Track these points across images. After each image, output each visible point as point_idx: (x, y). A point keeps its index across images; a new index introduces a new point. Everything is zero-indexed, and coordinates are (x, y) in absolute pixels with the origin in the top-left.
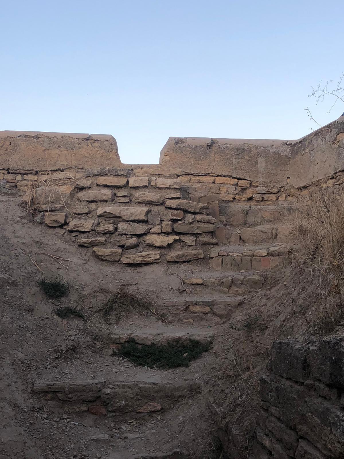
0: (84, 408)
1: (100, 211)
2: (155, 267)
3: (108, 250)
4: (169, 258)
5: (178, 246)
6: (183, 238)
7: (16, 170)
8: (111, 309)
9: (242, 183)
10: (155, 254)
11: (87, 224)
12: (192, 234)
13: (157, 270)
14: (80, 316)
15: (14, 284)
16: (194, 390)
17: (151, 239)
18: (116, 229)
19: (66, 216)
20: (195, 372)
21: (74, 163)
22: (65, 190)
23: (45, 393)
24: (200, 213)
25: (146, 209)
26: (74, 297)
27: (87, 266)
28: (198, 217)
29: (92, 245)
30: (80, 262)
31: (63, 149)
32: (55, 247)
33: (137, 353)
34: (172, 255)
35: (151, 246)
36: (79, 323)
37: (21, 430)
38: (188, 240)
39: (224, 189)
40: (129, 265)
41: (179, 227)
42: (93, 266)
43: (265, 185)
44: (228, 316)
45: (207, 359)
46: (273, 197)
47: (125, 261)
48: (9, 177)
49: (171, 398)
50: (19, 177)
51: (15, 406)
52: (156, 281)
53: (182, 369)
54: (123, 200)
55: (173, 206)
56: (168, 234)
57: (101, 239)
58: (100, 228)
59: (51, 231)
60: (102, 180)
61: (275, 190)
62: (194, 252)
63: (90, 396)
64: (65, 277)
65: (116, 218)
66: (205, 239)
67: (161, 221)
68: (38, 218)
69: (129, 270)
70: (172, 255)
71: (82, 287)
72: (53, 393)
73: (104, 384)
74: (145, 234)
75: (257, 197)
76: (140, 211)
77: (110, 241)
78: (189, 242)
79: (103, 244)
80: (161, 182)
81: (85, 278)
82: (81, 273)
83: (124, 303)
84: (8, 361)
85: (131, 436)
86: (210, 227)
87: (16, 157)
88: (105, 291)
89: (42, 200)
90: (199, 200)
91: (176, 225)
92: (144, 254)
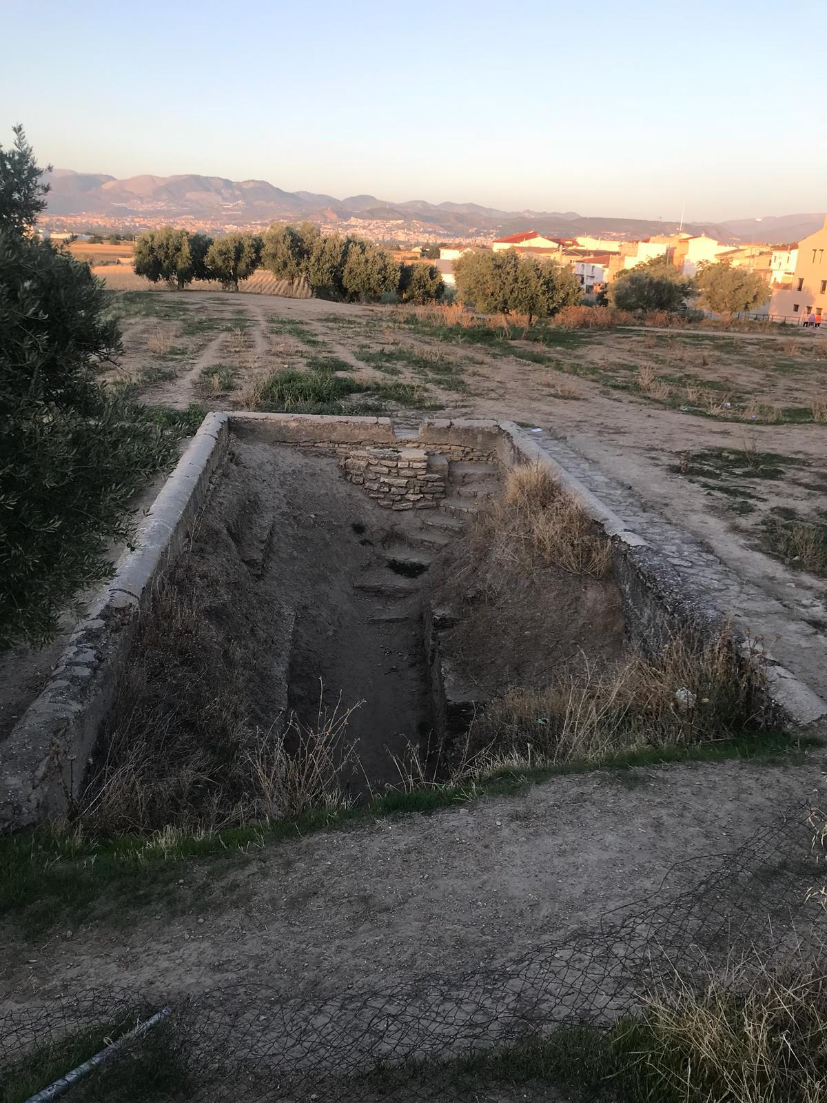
2: (410, 512)
3: (386, 503)
4: (417, 507)
7: (316, 335)
8: (386, 540)
10: (410, 505)
15: (340, 527)
16: (417, 590)
18: (390, 490)
20: (418, 582)
22: (363, 463)
25: (406, 481)
26: (368, 532)
28: (435, 484)
29: (377, 498)
34: (420, 504)
35: (409, 500)
36: (370, 547)
38: (429, 497)
42: (377, 511)
43: (481, 451)
46: (485, 459)
48: (331, 445)
49: (408, 593)
50: (336, 446)
51: (348, 594)
52: (408, 521)
53: (414, 579)
56: (417, 494)
57: (382, 496)
58: (381, 490)
59: (355, 487)
60: (383, 462)
61: (486, 455)
62: (431, 503)
64: (365, 520)
65: (390, 486)
68: (349, 478)
69: (396, 513)
70: (420, 504)
71: (372, 526)
72: (361, 588)
73: (382, 585)
75: (475, 458)
79: (383, 499)
80: (415, 465)
81: (374, 520)
82: (373, 517)
83: (393, 537)
85: (391, 608)
87: (334, 434)
88: (382, 529)
89: (351, 467)
90: (436, 472)
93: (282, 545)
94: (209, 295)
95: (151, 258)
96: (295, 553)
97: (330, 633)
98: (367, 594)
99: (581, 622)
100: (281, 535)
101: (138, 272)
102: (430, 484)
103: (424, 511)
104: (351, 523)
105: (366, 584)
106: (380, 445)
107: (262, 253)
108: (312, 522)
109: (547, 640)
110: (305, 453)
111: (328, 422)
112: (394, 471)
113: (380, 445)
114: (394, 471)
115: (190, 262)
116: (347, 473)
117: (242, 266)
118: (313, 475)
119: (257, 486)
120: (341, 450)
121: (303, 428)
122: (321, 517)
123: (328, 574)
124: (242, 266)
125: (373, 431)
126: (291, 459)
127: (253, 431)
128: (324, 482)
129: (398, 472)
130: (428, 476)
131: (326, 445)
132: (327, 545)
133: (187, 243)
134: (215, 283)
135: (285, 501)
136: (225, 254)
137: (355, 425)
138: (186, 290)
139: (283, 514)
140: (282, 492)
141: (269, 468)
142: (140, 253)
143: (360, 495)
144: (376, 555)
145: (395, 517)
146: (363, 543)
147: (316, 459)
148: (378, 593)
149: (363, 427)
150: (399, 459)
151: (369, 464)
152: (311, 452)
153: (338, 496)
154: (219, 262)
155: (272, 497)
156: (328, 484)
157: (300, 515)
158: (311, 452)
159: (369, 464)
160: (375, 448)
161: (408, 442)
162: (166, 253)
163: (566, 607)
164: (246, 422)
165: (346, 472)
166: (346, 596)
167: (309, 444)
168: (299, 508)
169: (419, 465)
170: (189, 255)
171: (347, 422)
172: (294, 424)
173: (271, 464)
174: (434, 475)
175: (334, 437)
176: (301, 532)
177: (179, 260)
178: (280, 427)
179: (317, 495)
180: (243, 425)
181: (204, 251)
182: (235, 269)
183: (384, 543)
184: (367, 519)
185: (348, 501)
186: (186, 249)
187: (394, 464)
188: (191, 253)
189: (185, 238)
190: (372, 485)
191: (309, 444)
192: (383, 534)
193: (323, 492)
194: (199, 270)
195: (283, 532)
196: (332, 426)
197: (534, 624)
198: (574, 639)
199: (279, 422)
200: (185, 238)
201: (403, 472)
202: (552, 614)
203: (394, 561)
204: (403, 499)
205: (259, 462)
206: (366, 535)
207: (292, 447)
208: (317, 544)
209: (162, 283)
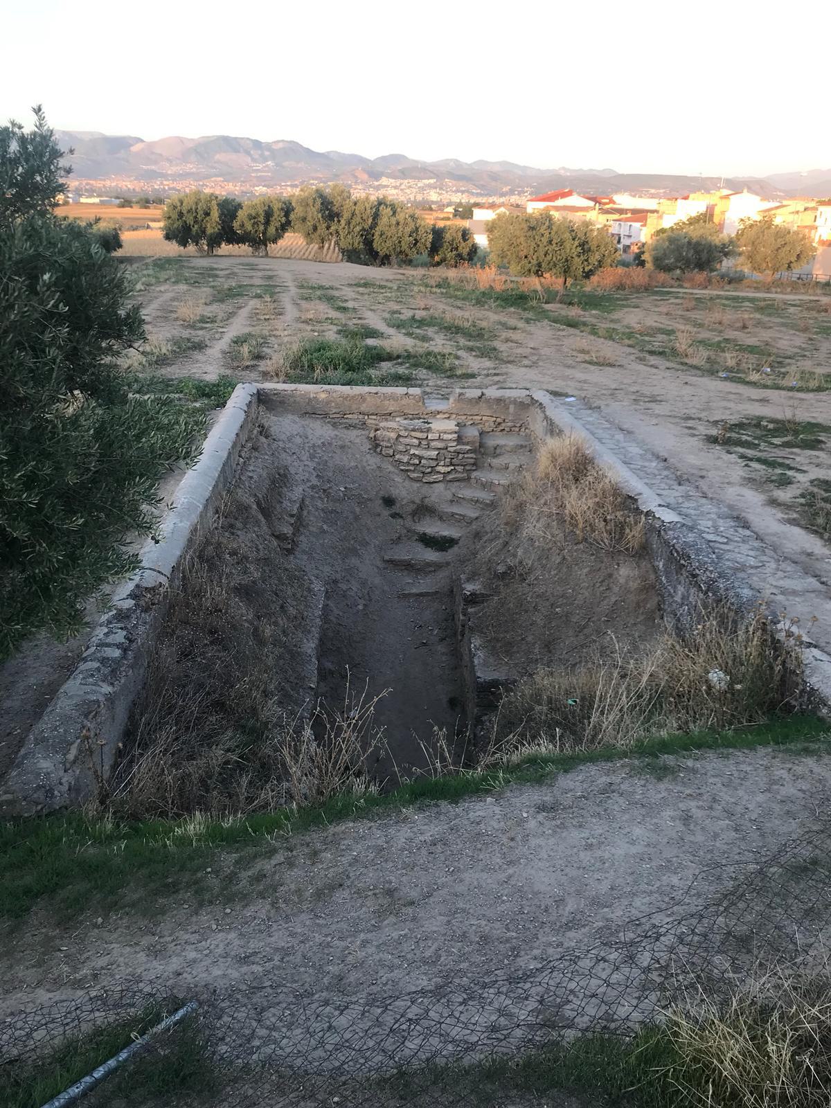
1: (412, 452)
2: (440, 484)
3: (416, 475)
7: (346, 301)
9: (499, 420)
10: (440, 477)
14: (401, 517)
15: (370, 500)
16: (448, 564)
17: (439, 469)
22: (393, 435)
26: (398, 505)
29: (407, 471)
33: (428, 541)
34: (450, 477)
35: (439, 472)
38: (460, 468)
39: (487, 424)
42: (407, 483)
44: (470, 523)
45: (455, 549)
48: (361, 417)
49: (438, 566)
52: (438, 494)
57: (412, 468)
60: (413, 434)
65: (420, 458)
66: (468, 468)
68: (378, 450)
69: (426, 485)
70: (450, 477)
72: (391, 561)
77: (419, 471)
80: (446, 437)
81: (404, 493)
82: (403, 490)
83: (424, 510)
86: (472, 461)
88: (413, 502)
90: (468, 444)
95: (180, 223)
99: (613, 599)
107: (292, 217)
110: (334, 425)
112: (424, 442)
114: (424, 442)
116: (377, 445)
117: (272, 230)
118: (342, 447)
119: (286, 459)
120: (371, 421)
124: (272, 230)
125: (403, 402)
126: (320, 431)
127: (282, 402)
129: (428, 444)
132: (357, 518)
133: (216, 207)
134: (245, 248)
135: (315, 474)
140: (312, 465)
141: (298, 440)
142: (169, 218)
143: (391, 468)
145: (425, 490)
147: (346, 431)
150: (429, 430)
151: (399, 436)
152: (341, 424)
153: (368, 468)
158: (341, 424)
159: (399, 436)
161: (439, 413)
162: (196, 217)
165: (375, 444)
168: (329, 481)
169: (450, 437)
172: (323, 396)
175: (364, 408)
176: (330, 506)
177: (208, 226)
178: (310, 399)
181: (233, 216)
186: (215, 214)
187: (425, 435)
193: (353, 464)
194: (228, 234)
200: (214, 202)
204: (433, 471)
206: (396, 509)
208: (347, 518)
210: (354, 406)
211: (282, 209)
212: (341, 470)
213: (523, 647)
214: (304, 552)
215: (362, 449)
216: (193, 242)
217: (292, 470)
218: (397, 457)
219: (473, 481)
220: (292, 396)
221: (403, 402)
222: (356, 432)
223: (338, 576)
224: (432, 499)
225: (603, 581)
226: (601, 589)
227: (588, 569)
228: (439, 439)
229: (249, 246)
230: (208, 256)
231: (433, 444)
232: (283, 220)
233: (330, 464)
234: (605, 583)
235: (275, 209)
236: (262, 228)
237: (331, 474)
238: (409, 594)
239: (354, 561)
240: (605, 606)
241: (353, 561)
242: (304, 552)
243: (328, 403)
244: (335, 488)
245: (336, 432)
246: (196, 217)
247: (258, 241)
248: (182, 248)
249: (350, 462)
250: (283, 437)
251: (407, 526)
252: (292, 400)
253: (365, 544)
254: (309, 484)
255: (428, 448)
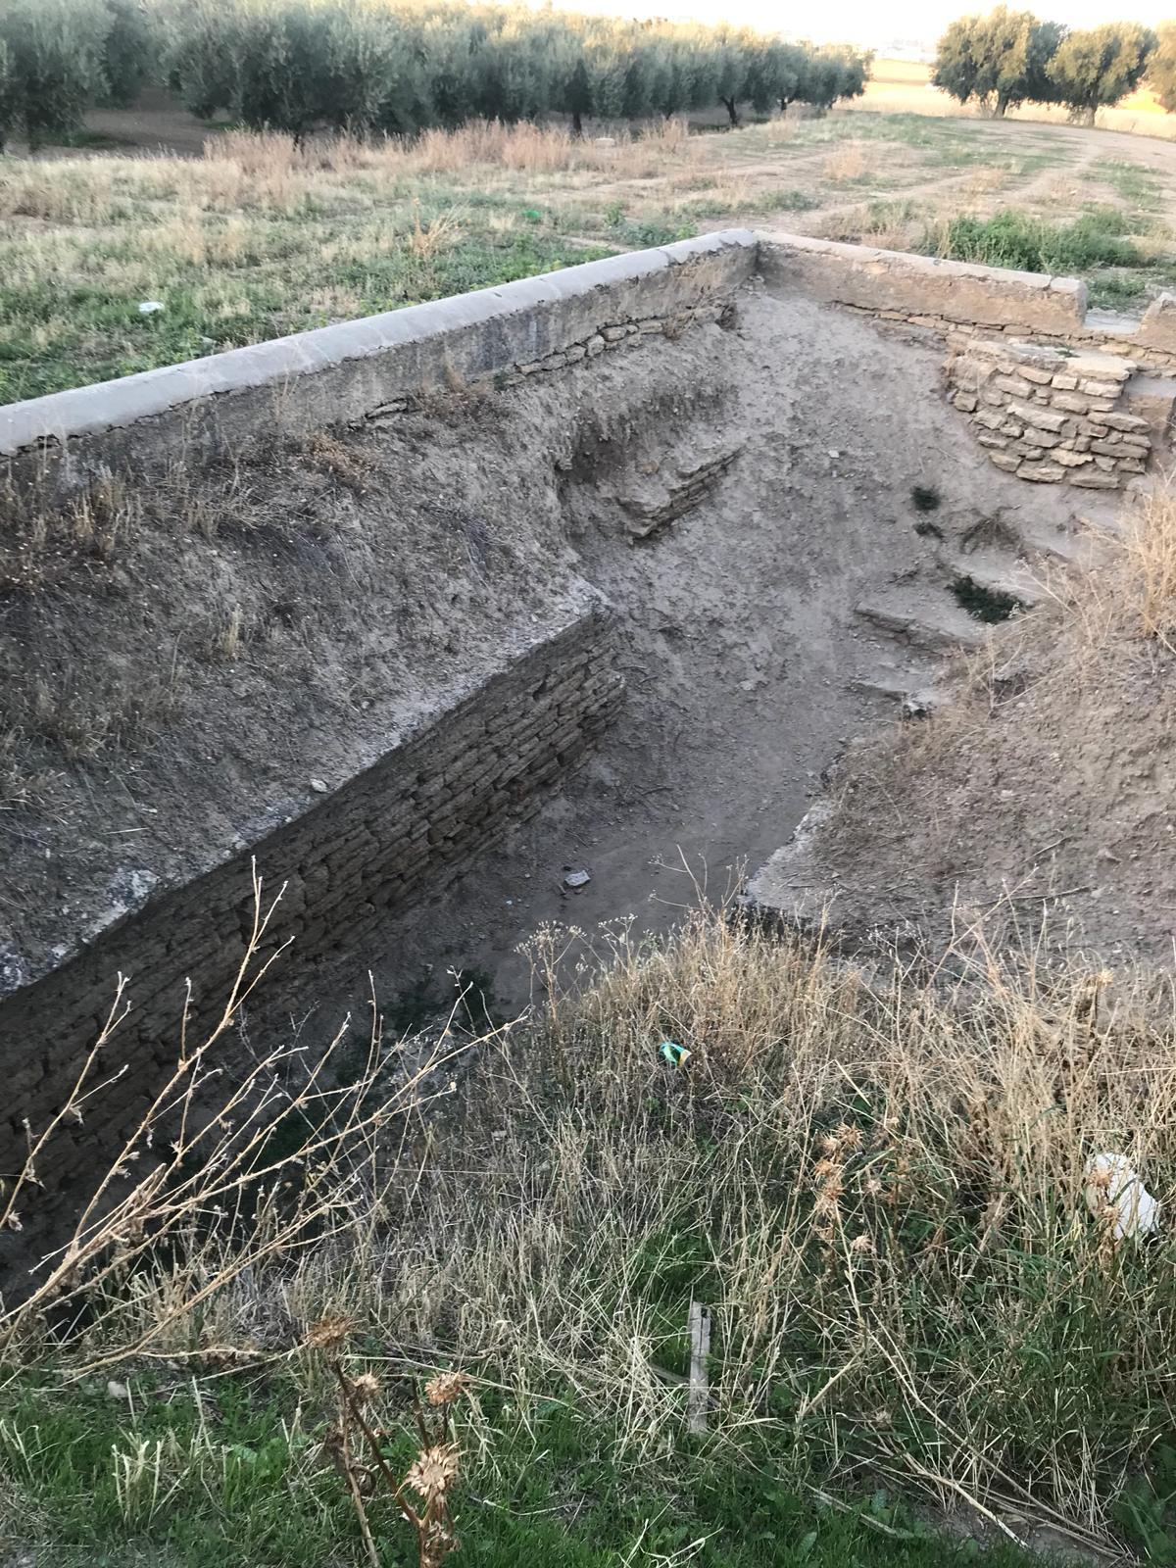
0: (891, 635)
1: (1010, 410)
5: (1089, 468)
6: (1099, 460)
10: (1057, 473)
11: (994, 420)
12: (1113, 457)
13: (1051, 493)
15: (888, 488)
18: (1022, 434)
19: (977, 403)
21: (1020, 318)
22: (985, 369)
23: (864, 614)
24: (1132, 432)
25: (1062, 418)
26: (942, 511)
27: (976, 473)
28: (1127, 437)
29: (992, 446)
30: (972, 465)
31: (1011, 298)
32: (953, 440)
34: (1079, 477)
37: (831, 642)
38: (1105, 463)
40: (1024, 479)
41: (1098, 445)
42: (982, 475)
47: (1021, 474)
48: (941, 325)
50: (952, 327)
51: (836, 621)
54: (1040, 401)
55: (1096, 421)
56: (1081, 452)
57: (1002, 443)
58: (1004, 430)
59: (959, 415)
60: (1024, 370)
62: (1107, 479)
63: (899, 628)
64: (946, 485)
66: (1124, 465)
67: (1078, 434)
69: (1023, 485)
70: (1079, 477)
72: (869, 616)
73: (913, 622)
74: (1053, 448)
76: (1054, 419)
78: (1104, 467)
79: (1005, 449)
80: (1092, 387)
81: (966, 490)
82: (968, 485)
84: (847, 577)
86: (1139, 452)
87: (953, 301)
88: (976, 512)
89: (960, 372)
90: (1141, 413)
91: (1095, 443)
92: (1044, 470)
93: (737, 494)
94: (1035, 128)
95: (962, 59)
96: (757, 517)
97: (748, 685)
98: (878, 632)
99: (1147, 808)
100: (746, 475)
101: (937, 82)
102: (1115, 436)
103: (1087, 492)
104: (914, 484)
105: (883, 611)
106: (1043, 339)
107: (1150, 58)
108: (827, 463)
109: (1044, 827)
110: (884, 334)
111: (946, 273)
112: (1041, 392)
113: (1043, 339)
114: (1041, 392)
115: (1024, 70)
116: (951, 386)
117: (1110, 78)
118: (877, 377)
119: (742, 374)
120: (956, 337)
121: (892, 279)
122: (854, 459)
123: (813, 573)
124: (1110, 78)
125: (1034, 306)
126: (849, 337)
127: (797, 274)
128: (894, 395)
129: (1049, 398)
130: (1114, 416)
131: (930, 322)
132: (840, 516)
133: (1025, 34)
134: (1058, 111)
135: (790, 413)
136: (1085, 56)
137: (1000, 288)
138: (1006, 119)
139: (771, 438)
140: (792, 395)
141: (792, 346)
142: (947, 49)
143: (961, 435)
144: (938, 560)
145: (1017, 493)
146: (923, 530)
147: (900, 348)
148: (901, 634)
149: (1016, 292)
150: (1059, 368)
151: (997, 373)
152: (897, 333)
153: (912, 426)
154: (1071, 73)
155: (764, 402)
156: (901, 399)
157: (808, 446)
158: (897, 333)
159: (997, 373)
160: (1028, 342)
161: (1107, 340)
162: (989, 50)
163: (1125, 757)
164: (788, 256)
165: (948, 384)
166: (828, 624)
167: (896, 316)
168: (813, 433)
169: (1100, 388)
170: (1023, 55)
171: (983, 279)
172: (876, 270)
173: (800, 342)
174: (1129, 418)
175: (951, 307)
176: (794, 480)
177: (1006, 65)
178: (849, 274)
179: (867, 416)
180: (781, 261)
181: (1050, 50)
182: (1095, 84)
183: (966, 540)
184: (955, 483)
185: (930, 441)
186: (1022, 46)
187: (1045, 377)
188: (1028, 52)
189: (1025, 25)
190: (989, 416)
191: (896, 316)
192: (972, 521)
193: (882, 411)
194: (1037, 86)
195: (752, 473)
196: (952, 282)
197: (1030, 778)
198: (1111, 847)
199: (849, 261)
200: (1025, 25)
201: (1058, 398)
202: (1084, 764)
203: (969, 579)
204: (1044, 455)
205: (777, 332)
206: (935, 517)
207: (865, 316)
208: (818, 511)
209: (973, 103)
210: (933, 301)
211: (1137, 44)
212: (853, 421)
213: (892, 859)
214: (681, 552)
215: (918, 387)
216: (977, 92)
217: (745, 397)
218: (979, 415)
219: (1128, 496)
220: (817, 263)
221: (1034, 306)
222: (919, 353)
223: (730, 615)
224: (1022, 514)
225: (1142, 752)
226: (1128, 771)
227: (1115, 709)
228: (1076, 389)
229: (1067, 106)
230: (994, 118)
231: (1059, 399)
232: (1134, 63)
233: (834, 402)
234: (1144, 761)
235: (1125, 44)
236: (1093, 74)
237: (825, 421)
238: (871, 689)
239: (789, 596)
240: (1120, 822)
241: (785, 596)
242: (681, 552)
243: (883, 285)
244: (819, 448)
245: (879, 347)
246: (989, 50)
247: (1085, 96)
248: (957, 101)
249: (878, 406)
250: (764, 335)
251: (944, 556)
252: (816, 270)
253: (831, 569)
254: (768, 429)
255: (1048, 404)
